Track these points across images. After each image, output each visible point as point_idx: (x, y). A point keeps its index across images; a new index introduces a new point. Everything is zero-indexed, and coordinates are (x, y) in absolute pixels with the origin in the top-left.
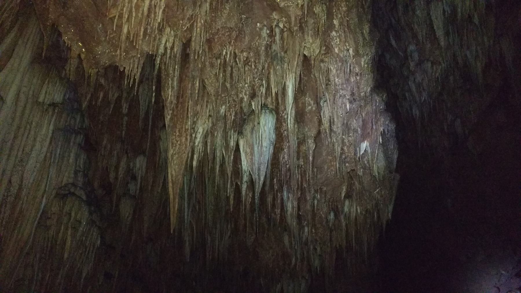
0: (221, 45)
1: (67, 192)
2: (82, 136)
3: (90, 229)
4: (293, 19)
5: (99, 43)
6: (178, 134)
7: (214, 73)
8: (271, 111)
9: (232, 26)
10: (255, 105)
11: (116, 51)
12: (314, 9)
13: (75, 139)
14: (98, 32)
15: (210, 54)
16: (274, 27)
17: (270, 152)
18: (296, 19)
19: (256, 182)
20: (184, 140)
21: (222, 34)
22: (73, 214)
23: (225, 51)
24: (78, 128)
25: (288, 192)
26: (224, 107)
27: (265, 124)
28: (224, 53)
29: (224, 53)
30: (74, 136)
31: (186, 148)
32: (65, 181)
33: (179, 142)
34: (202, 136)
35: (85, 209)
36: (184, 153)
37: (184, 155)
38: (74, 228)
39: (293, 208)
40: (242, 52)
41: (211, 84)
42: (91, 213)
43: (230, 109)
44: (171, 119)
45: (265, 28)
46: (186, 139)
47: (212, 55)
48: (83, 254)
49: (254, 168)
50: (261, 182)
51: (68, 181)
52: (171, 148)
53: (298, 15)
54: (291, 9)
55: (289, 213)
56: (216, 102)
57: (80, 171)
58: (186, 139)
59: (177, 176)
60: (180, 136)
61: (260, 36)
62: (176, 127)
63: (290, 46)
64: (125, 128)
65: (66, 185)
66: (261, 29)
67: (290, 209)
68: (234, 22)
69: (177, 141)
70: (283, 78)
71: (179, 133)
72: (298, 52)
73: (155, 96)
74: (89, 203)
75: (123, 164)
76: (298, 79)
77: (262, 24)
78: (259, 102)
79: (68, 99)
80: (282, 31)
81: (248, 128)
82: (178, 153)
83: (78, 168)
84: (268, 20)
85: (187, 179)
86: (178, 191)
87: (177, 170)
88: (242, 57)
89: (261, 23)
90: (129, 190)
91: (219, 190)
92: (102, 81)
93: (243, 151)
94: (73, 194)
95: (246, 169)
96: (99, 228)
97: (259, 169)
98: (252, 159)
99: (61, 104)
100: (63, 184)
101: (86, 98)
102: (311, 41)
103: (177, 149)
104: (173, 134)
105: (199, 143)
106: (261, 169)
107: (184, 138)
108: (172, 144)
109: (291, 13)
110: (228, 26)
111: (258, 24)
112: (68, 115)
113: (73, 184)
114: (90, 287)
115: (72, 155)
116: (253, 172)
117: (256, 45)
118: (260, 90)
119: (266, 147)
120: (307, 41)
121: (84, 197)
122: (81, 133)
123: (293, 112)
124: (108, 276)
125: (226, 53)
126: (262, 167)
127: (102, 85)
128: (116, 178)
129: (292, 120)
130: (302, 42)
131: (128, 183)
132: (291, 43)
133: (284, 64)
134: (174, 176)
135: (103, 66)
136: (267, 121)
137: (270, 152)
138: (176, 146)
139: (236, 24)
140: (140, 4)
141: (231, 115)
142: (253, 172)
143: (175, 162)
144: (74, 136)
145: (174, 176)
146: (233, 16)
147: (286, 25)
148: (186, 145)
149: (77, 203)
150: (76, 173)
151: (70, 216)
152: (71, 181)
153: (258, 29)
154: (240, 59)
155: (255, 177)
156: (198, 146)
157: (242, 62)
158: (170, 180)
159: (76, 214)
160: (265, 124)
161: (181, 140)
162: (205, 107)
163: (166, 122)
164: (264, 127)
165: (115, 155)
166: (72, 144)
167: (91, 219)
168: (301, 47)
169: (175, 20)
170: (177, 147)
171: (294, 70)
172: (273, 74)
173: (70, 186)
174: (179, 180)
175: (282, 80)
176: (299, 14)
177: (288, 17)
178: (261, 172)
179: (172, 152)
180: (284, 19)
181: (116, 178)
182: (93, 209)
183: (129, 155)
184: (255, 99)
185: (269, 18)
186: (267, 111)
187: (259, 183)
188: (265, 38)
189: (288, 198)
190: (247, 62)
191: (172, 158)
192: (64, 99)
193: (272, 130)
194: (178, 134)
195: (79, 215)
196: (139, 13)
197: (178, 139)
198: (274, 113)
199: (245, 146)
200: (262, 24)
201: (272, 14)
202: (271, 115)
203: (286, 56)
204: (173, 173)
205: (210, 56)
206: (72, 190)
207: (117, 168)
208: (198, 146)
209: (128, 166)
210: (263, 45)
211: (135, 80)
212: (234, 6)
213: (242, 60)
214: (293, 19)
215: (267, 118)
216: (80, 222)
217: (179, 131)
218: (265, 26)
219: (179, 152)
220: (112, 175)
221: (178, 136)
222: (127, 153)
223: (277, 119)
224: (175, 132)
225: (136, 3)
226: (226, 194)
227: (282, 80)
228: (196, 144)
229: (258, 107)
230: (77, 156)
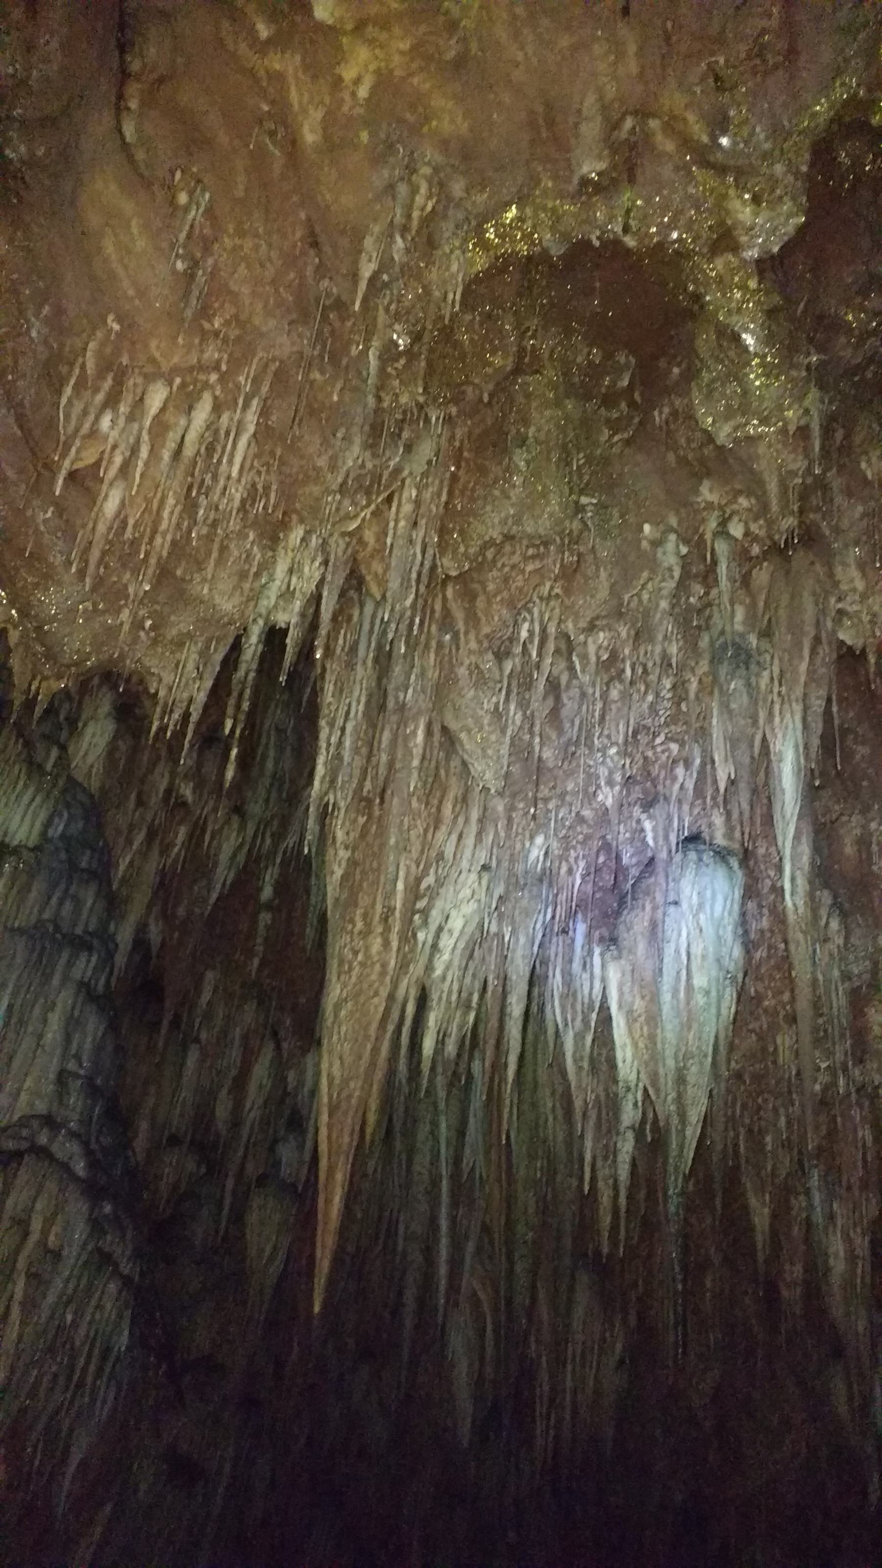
0: (511, 604)
1: (25, 1145)
2: (94, 959)
3: (90, 1284)
4: (773, 487)
5: (48, 577)
6: (360, 925)
7: (488, 705)
8: (722, 855)
9: (542, 531)
10: (654, 829)
11: (118, 611)
12: (863, 465)
13: (70, 965)
14: (37, 529)
15: (472, 636)
16: (708, 536)
17: (724, 1012)
18: (784, 488)
19: (668, 1131)
20: (376, 944)
21: (513, 567)
22: (36, 1225)
23: (526, 626)
24: (86, 931)
25: (831, 1196)
26: (539, 840)
27: (701, 906)
28: (524, 634)
29: (524, 634)
30: (65, 956)
31: (383, 973)
32: (22, 1106)
33: (360, 957)
34: (461, 945)
35: (78, 1208)
36: (376, 994)
37: (376, 1000)
38: (36, 1276)
39: (852, 1258)
40: (592, 628)
41: (484, 750)
42: (96, 1226)
43: (567, 849)
44: (345, 877)
45: (673, 537)
46: (386, 944)
47: (480, 642)
48: (61, 1381)
49: (661, 1071)
50: (689, 1132)
51: (31, 1105)
52: (334, 979)
53: (793, 474)
54: (761, 449)
55: (836, 1280)
56: (510, 820)
57: (77, 1076)
58: (386, 944)
59: (346, 1081)
60: (366, 933)
61: (653, 564)
62: (356, 905)
63: (781, 612)
64: (260, 949)
65: (24, 1121)
66: (657, 543)
67: (838, 1265)
68: (551, 515)
69: (356, 953)
70: (755, 722)
71: (365, 924)
72: (811, 631)
73: (238, 756)
74: (93, 1191)
75: (261, 1072)
76: (818, 727)
77: (662, 527)
78: (669, 818)
79: (63, 837)
80: (742, 555)
81: (637, 922)
82: (357, 995)
83: (72, 1066)
84: (683, 511)
85: (448, 1127)
86: (346, 1139)
87: (348, 1060)
88: (592, 649)
89: (655, 524)
90: (277, 1164)
91: (551, 1172)
92: (187, 791)
93: (620, 1007)
94: (43, 1153)
95: (633, 1077)
96: (127, 1281)
97: (681, 1080)
98: (652, 1038)
99: (32, 850)
100: (16, 1117)
101: (129, 842)
102: (860, 585)
103: (354, 979)
104: (343, 928)
105: (447, 968)
106: (691, 1079)
107: (379, 940)
108: (341, 963)
109: (764, 464)
110: (529, 530)
111: (647, 528)
112: (54, 886)
113: (49, 1121)
114: (108, 1508)
115: (55, 1020)
116: (657, 1091)
117: (640, 601)
118: (674, 779)
119: (707, 993)
120: (844, 587)
121: (80, 1168)
122: (90, 949)
123: (806, 849)
124: (183, 1470)
125: (531, 632)
126: (694, 1069)
127: (184, 804)
128: (236, 1123)
129: (801, 881)
130: (827, 594)
131: (276, 1141)
132: (785, 599)
133: (758, 675)
134: (337, 1081)
135: (76, 664)
136: (708, 893)
137: (724, 1012)
138: (351, 969)
139: (559, 522)
140: (172, 420)
141: (570, 871)
142: (657, 1091)
143: (344, 1029)
144: (65, 956)
145: (337, 1081)
146: (544, 495)
147: (754, 528)
148: (384, 966)
149: (52, 1186)
150: (62, 1078)
151: (26, 1234)
152: (41, 1107)
153: (645, 544)
154: (584, 657)
155: (667, 1107)
156: (444, 978)
157: (592, 667)
158: (325, 1100)
159: (49, 1222)
160: (701, 906)
161: (367, 948)
162: (470, 841)
163: (329, 889)
164: (696, 916)
165: (237, 1042)
166: (56, 981)
167: (99, 1250)
168: (824, 612)
169: (316, 490)
170: (354, 974)
171: (799, 691)
172: (721, 713)
173: (35, 1124)
174: (350, 1096)
175: (750, 731)
176: (793, 467)
177: (755, 486)
178: (690, 1091)
179: (338, 991)
180: (743, 502)
181: (236, 1123)
182: (108, 1209)
183: (285, 1045)
184: (658, 810)
185: (686, 504)
186: (708, 857)
187: (682, 1132)
188: (670, 569)
189: (831, 1217)
190: (611, 664)
191: (336, 1016)
192: (44, 834)
193: (730, 928)
194: (360, 925)
195: (55, 1229)
196: (163, 446)
197: (359, 944)
198: (734, 863)
199: (626, 989)
200: (662, 527)
201: (697, 492)
202: (721, 873)
203: (765, 645)
204: (336, 1071)
205: (473, 645)
206: (43, 1139)
207: (240, 1083)
208: (444, 978)
209: (279, 1079)
210: (665, 592)
211: (186, 716)
212: (548, 459)
213: (593, 659)
214: (773, 487)
215: (707, 879)
216: (57, 1255)
217: (365, 916)
218: (672, 530)
219: (357, 995)
220: (222, 1111)
221: (360, 933)
222: (275, 1034)
223: (750, 892)
224: (352, 921)
225: (157, 416)
226: (575, 1183)
227: (750, 731)
228: (438, 972)
229: (666, 837)
230: (72, 1024)
